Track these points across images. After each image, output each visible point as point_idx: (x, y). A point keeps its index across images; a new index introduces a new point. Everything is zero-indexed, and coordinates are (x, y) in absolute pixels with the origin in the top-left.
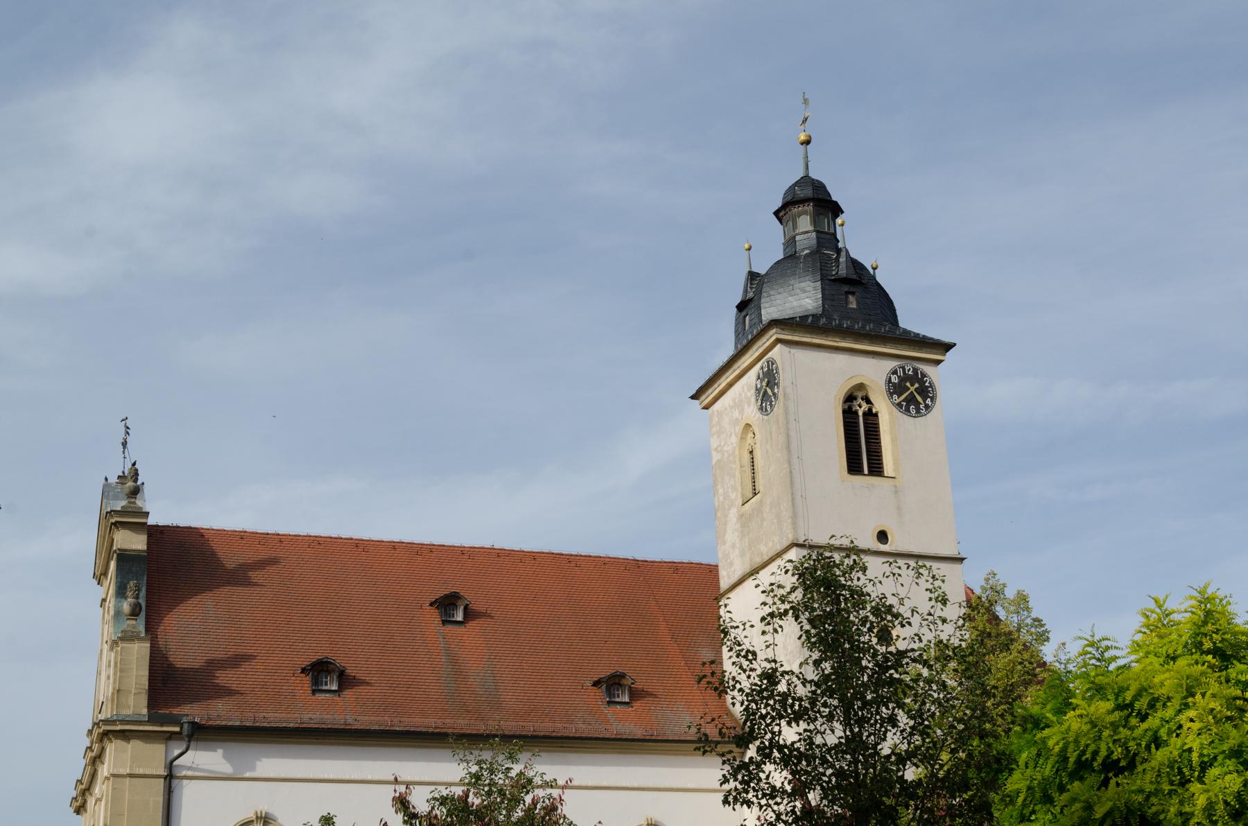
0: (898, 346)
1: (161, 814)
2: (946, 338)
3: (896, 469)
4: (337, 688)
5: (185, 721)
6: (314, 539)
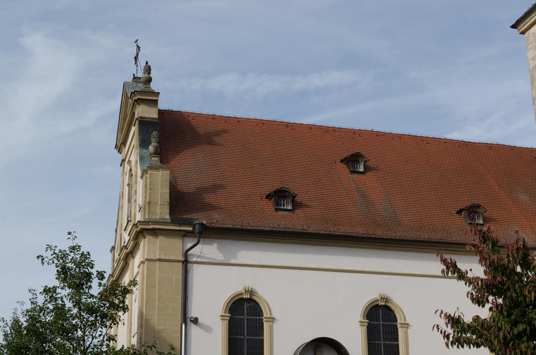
1: (181, 287)
4: (291, 208)
5: (197, 223)
6: (259, 121)
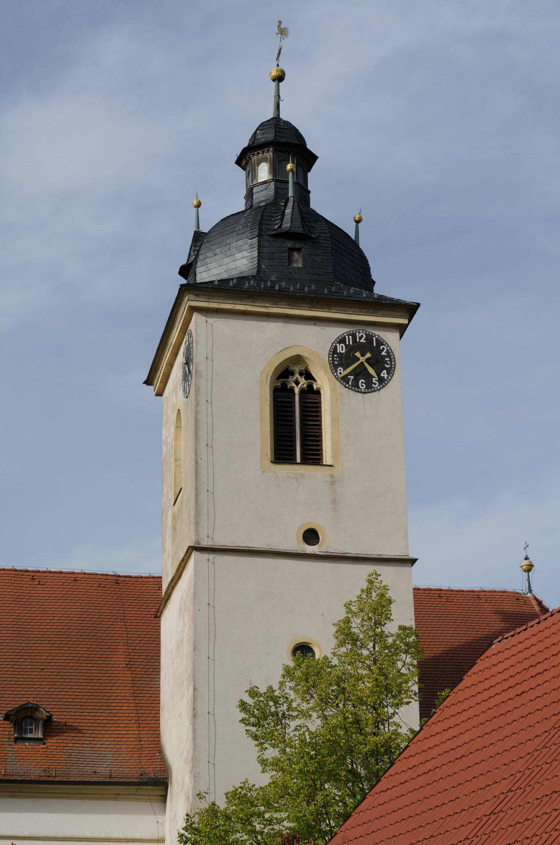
0: (346, 309)
2: (407, 297)
3: (335, 456)
4: (42, 737)
